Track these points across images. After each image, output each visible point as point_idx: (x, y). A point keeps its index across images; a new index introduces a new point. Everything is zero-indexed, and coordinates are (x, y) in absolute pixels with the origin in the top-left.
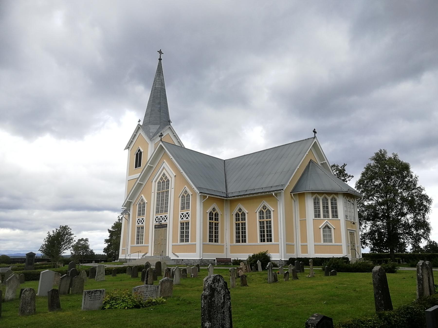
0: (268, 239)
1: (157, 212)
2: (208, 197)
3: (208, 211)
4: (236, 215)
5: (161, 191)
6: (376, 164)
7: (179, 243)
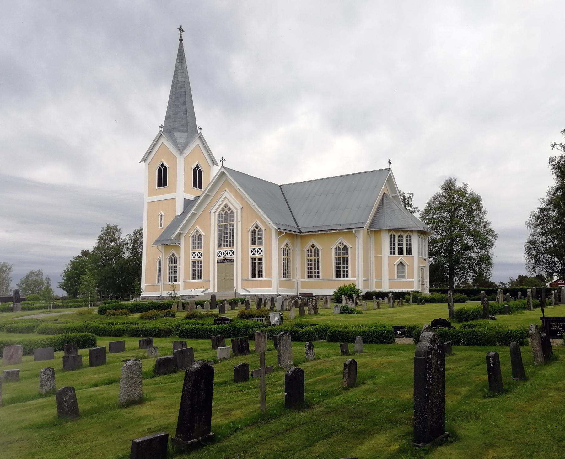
0: (259, 275)
1: (219, 246)
2: (284, 233)
3: (282, 247)
4: (308, 250)
5: (223, 223)
6: (444, 194)
7: (396, 279)
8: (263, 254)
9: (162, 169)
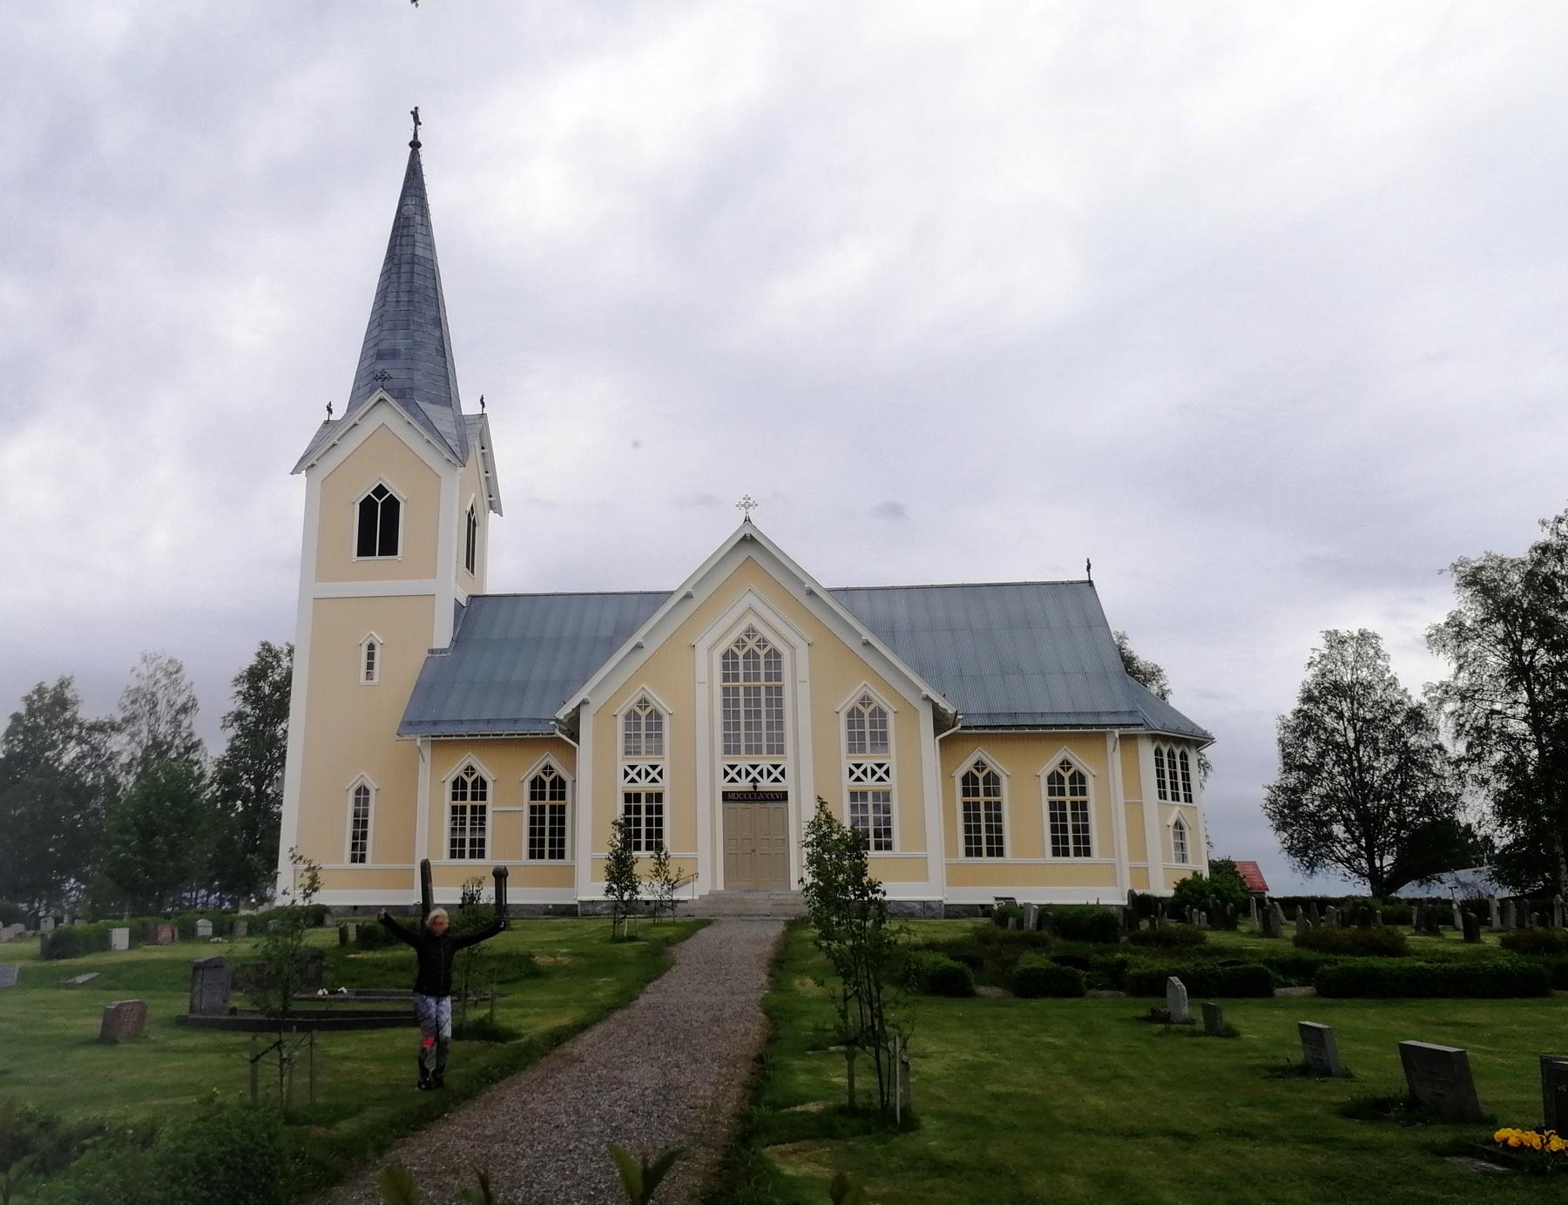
8: (892, 782)
9: (380, 502)
